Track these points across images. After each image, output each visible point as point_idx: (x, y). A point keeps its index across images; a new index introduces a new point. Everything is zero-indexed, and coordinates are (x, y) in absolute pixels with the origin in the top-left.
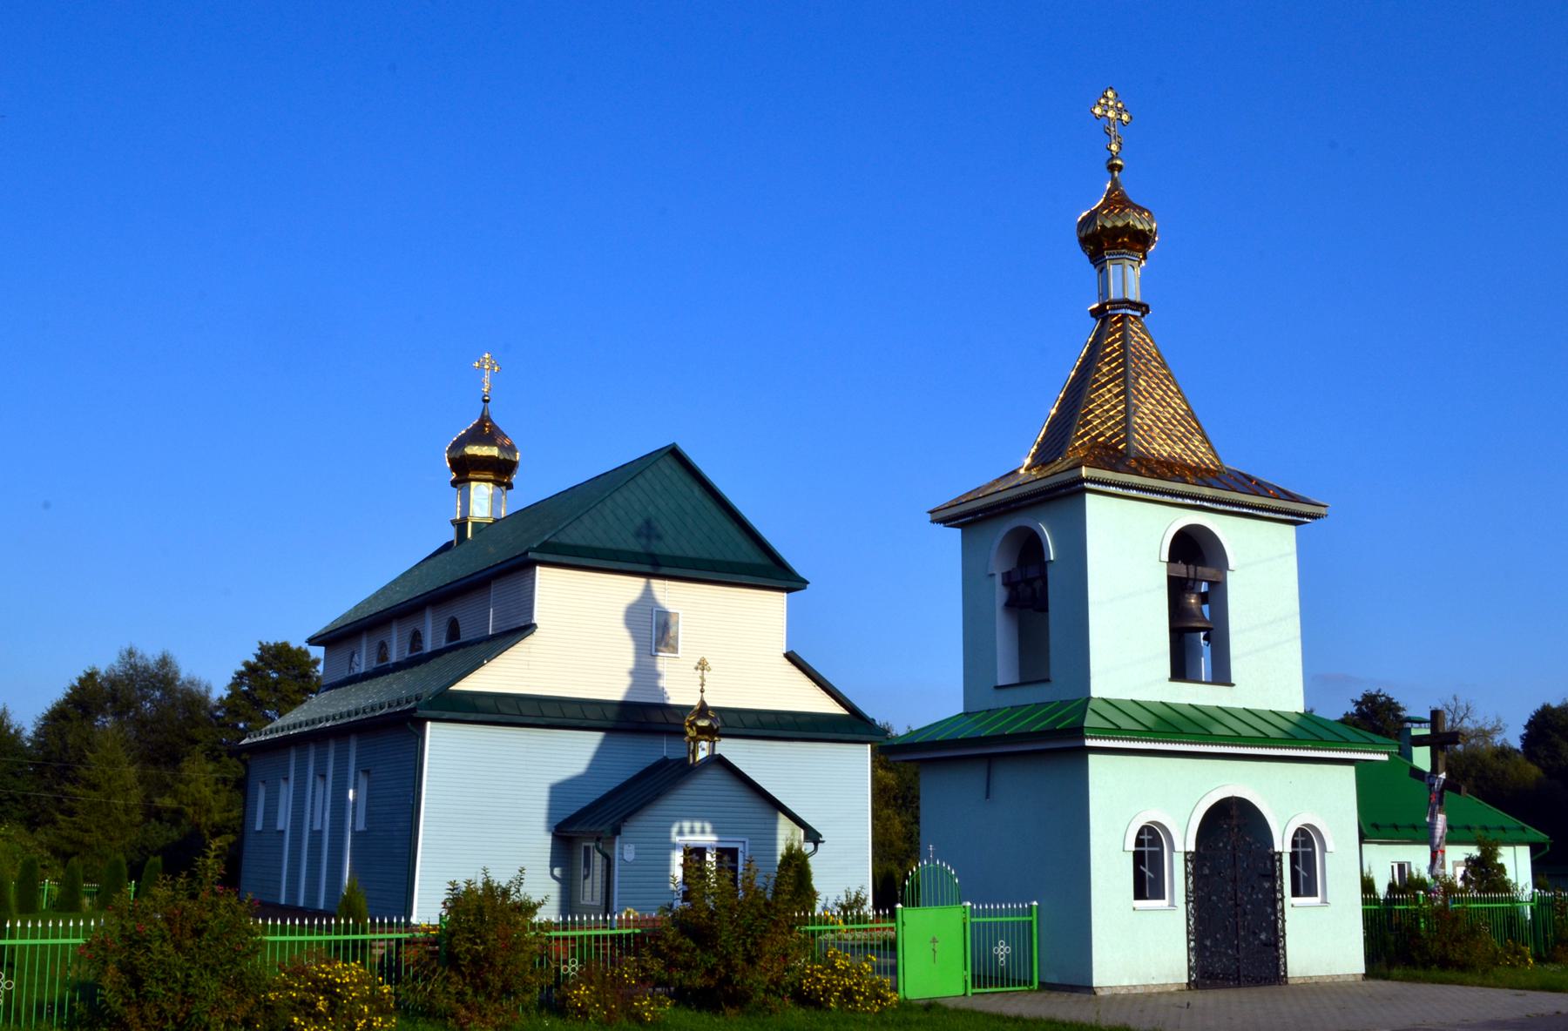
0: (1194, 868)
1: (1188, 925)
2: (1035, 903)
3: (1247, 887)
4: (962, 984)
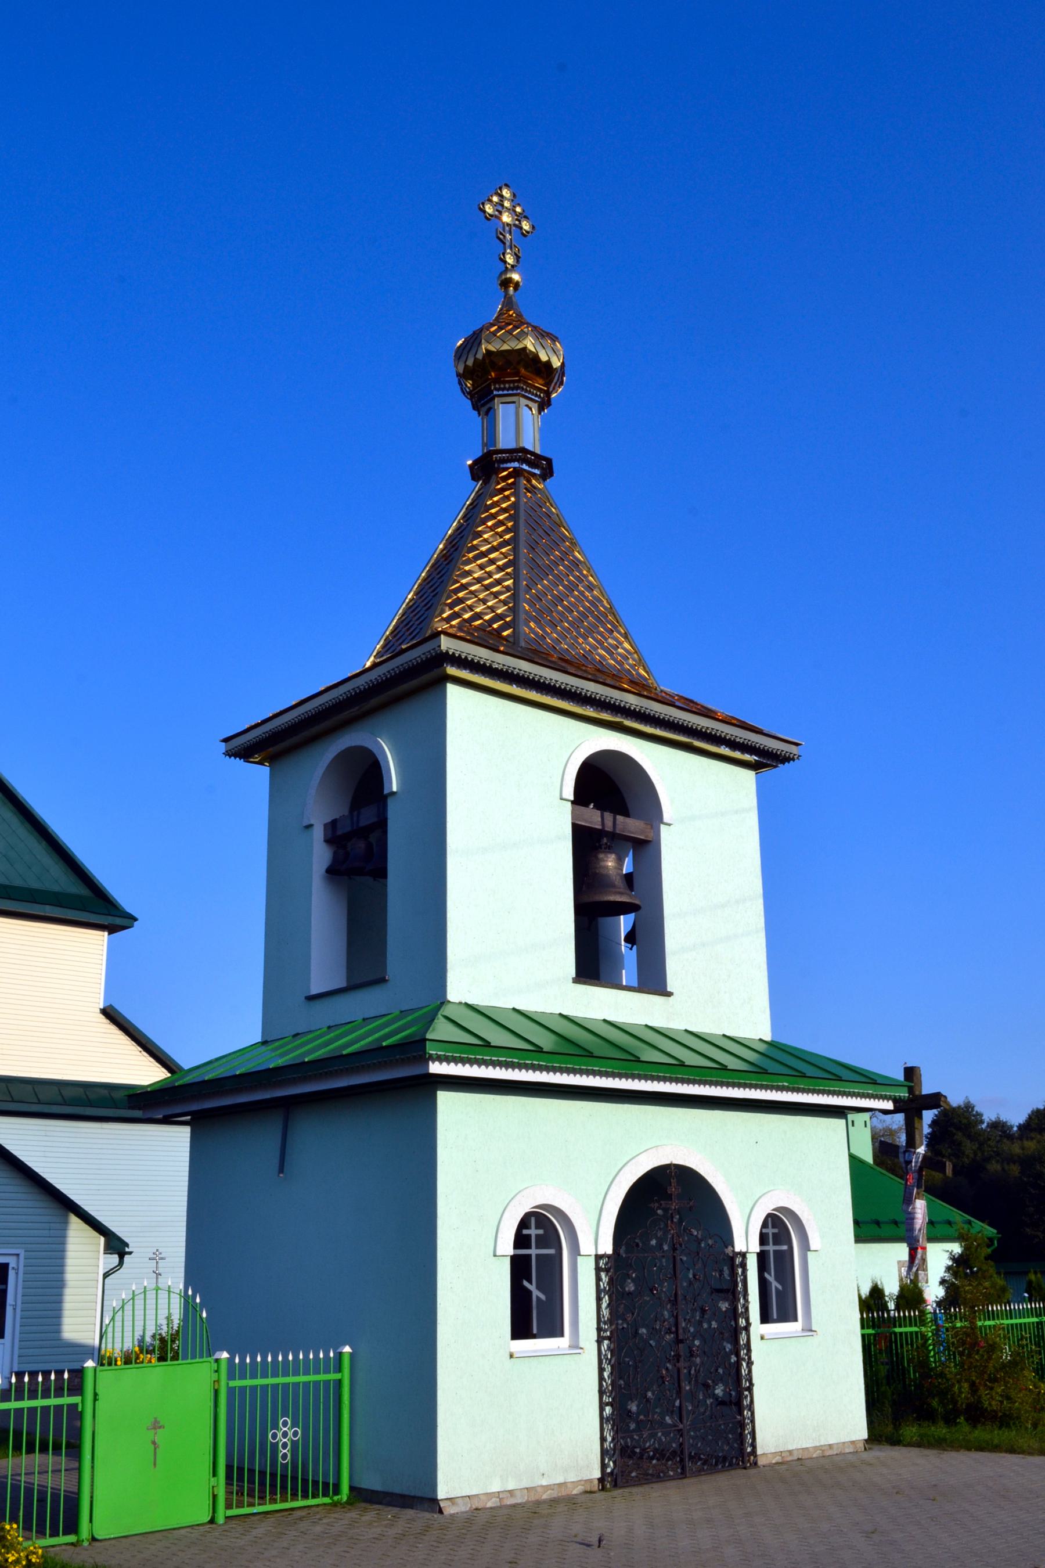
0: (611, 1282)
2: (347, 1349)
3: (694, 1310)
4: (207, 1502)
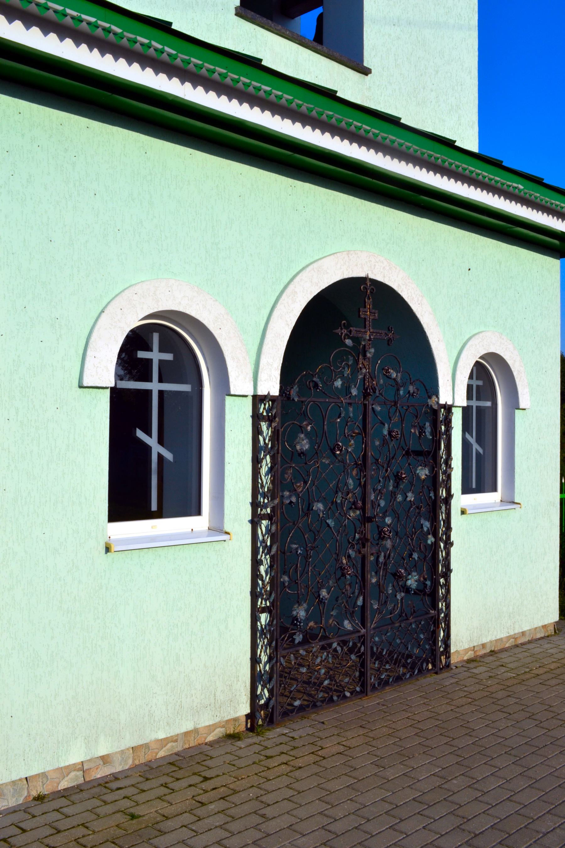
1: (255, 575)
3: (386, 478)
